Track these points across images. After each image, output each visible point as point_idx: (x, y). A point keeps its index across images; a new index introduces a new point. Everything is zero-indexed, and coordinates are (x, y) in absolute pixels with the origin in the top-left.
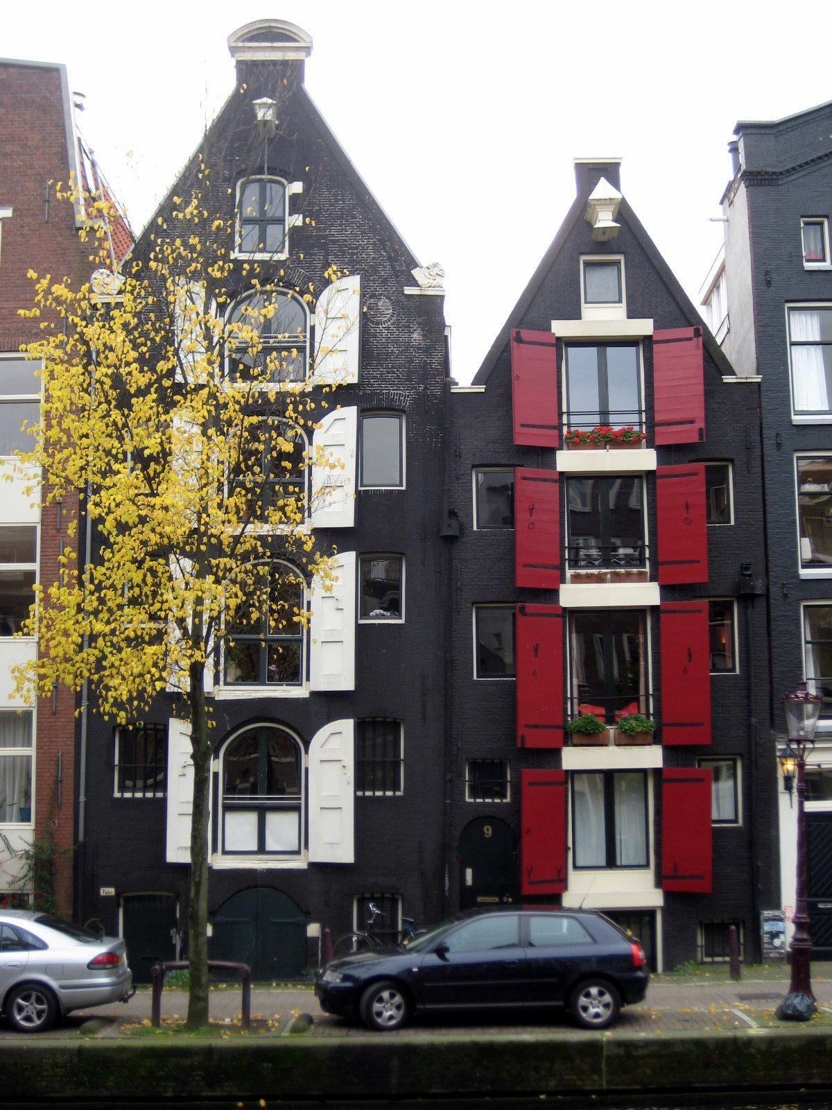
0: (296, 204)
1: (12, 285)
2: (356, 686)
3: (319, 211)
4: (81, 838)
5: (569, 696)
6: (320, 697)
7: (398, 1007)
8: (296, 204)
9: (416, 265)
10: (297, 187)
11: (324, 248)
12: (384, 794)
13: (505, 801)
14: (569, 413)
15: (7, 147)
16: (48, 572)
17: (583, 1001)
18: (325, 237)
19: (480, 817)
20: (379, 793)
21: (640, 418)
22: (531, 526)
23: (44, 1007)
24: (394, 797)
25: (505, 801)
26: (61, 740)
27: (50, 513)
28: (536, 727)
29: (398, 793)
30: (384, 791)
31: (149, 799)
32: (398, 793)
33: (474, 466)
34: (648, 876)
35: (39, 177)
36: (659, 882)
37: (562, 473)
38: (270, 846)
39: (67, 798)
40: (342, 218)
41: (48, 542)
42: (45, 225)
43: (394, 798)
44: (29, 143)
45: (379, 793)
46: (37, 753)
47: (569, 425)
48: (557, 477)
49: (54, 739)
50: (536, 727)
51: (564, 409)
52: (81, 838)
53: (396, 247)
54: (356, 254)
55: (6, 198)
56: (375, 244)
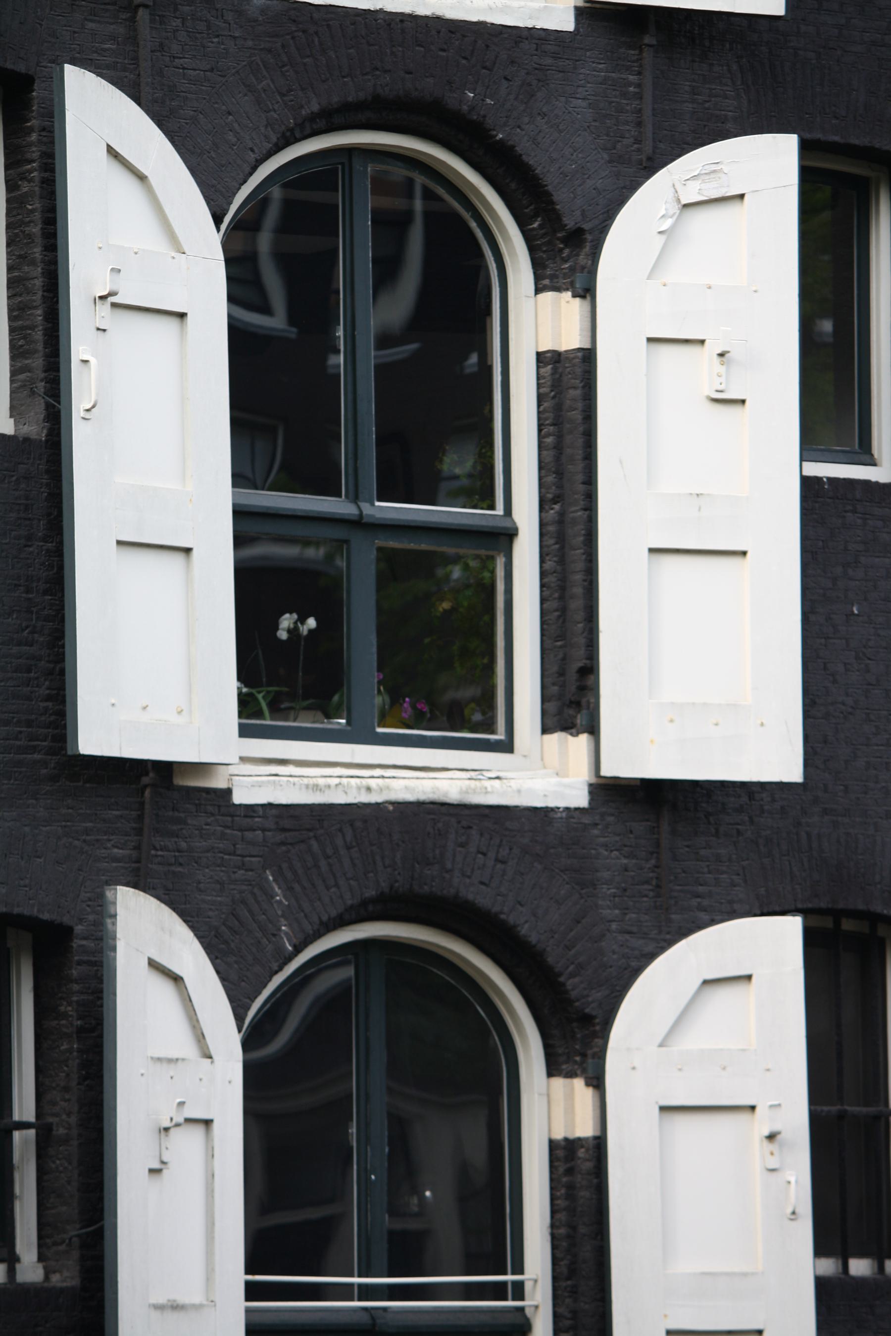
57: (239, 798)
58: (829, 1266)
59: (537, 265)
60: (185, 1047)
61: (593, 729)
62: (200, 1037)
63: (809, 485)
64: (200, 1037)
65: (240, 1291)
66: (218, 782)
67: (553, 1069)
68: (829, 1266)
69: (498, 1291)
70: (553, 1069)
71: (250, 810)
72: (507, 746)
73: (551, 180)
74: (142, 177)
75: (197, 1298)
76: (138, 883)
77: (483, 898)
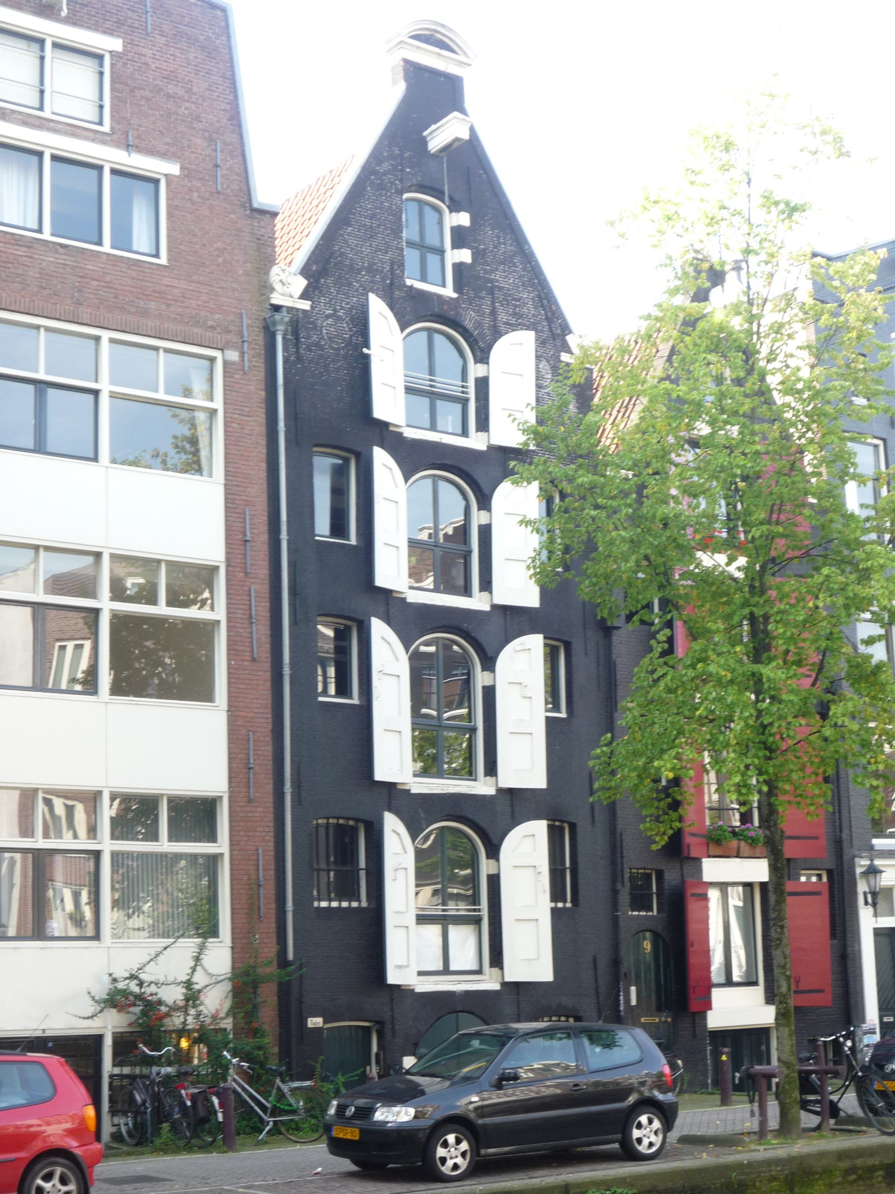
0: (460, 238)
1: (183, 260)
3: (484, 250)
6: (512, 794)
7: (464, 1155)
8: (460, 238)
9: (570, 332)
10: (463, 219)
11: (491, 291)
15: (170, 86)
16: (238, 625)
17: (441, 1152)
18: (492, 281)
23: (39, 1182)
26: (257, 834)
27: (237, 551)
30: (350, 901)
31: (560, 909)
34: (758, 993)
35: (207, 134)
36: (770, 998)
38: (453, 967)
39: (268, 907)
40: (503, 263)
41: (236, 587)
42: (216, 195)
43: (564, 908)
44: (195, 89)
46: (231, 850)
49: (251, 834)
53: (554, 308)
54: (519, 306)
55: (172, 150)
56: (533, 299)
57: (413, 791)
58: (553, 905)
59: (482, 665)
60: (401, 851)
61: (496, 775)
62: (404, 848)
63: (547, 718)
64: (404, 848)
65: (403, 375)
66: (403, 596)
67: (483, 670)
68: (553, 905)
69: (475, 910)
70: (483, 670)
71: (411, 604)
72: (475, 780)
73: (485, 645)
74: (389, 644)
75: (406, 964)
76: (390, 810)
77: (470, 816)
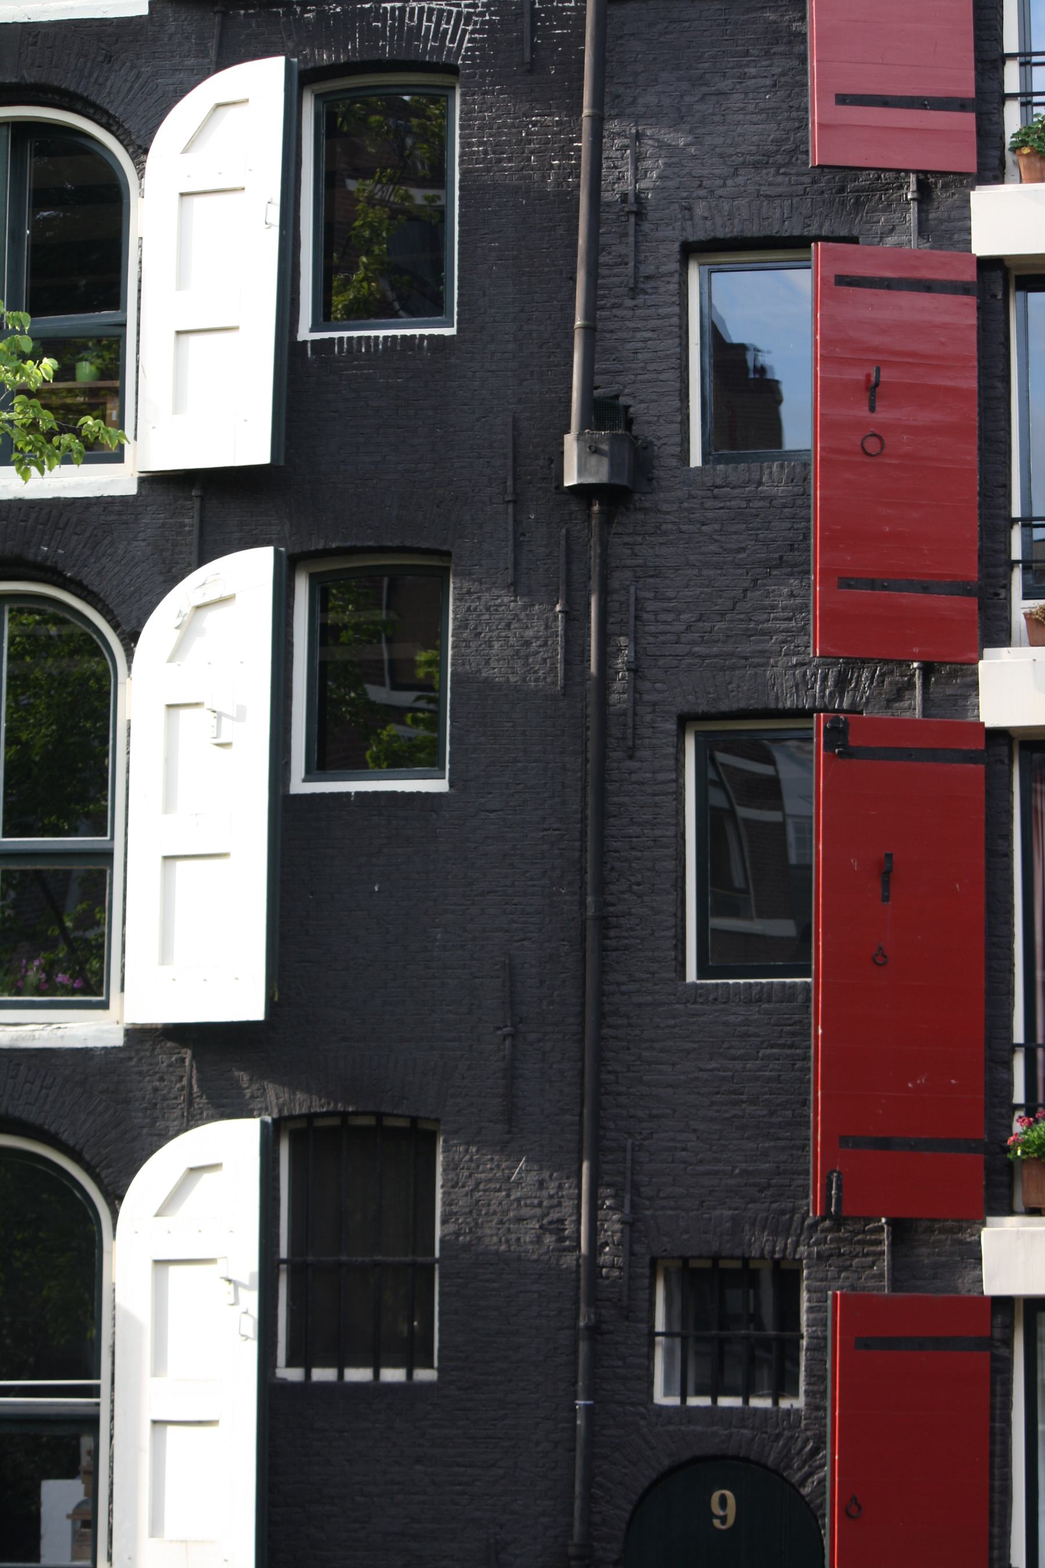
2: (271, 1004)
4: (751, 1292)
5: (1019, 1036)
12: (341, 1375)
13: (785, 1404)
14: (1026, 59)
19: (695, 1460)
20: (358, 1375)
21: (1026, 79)
22: (872, 446)
24: (409, 1387)
25: (785, 1404)
28: (884, 1144)
29: (425, 1375)
32: (425, 1375)
33: (689, 251)
37: (990, 265)
45: (358, 1375)
47: (1026, 98)
48: (970, 274)
50: (884, 1144)
51: (1011, 43)
52: (751, 1292)
